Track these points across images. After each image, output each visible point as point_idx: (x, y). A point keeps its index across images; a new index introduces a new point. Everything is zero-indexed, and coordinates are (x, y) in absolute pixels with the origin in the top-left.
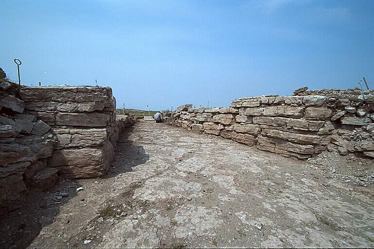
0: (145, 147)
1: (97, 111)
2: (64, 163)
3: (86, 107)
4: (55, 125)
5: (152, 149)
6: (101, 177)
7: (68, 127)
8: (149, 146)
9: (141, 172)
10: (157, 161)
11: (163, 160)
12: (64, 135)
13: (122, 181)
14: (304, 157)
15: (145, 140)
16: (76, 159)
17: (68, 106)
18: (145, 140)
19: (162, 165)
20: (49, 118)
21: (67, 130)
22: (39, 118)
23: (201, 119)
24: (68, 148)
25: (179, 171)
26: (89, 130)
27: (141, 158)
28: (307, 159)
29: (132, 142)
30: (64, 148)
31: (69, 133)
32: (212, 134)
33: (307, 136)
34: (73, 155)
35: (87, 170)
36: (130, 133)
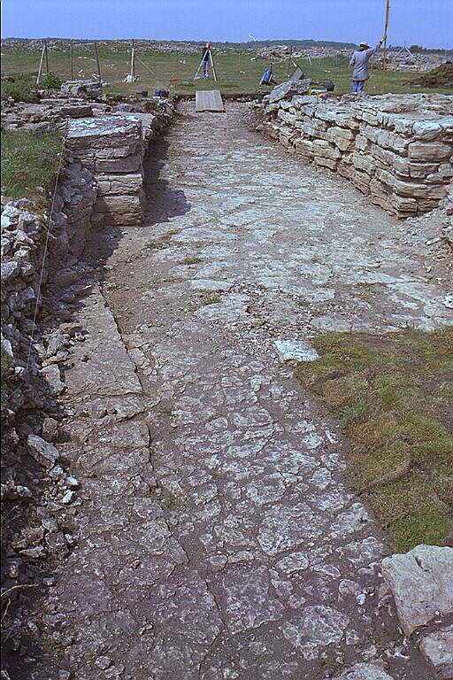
0: (187, 192)
1: (130, 155)
2: (106, 209)
3: (120, 152)
4: (95, 172)
5: (197, 196)
6: (139, 225)
7: (106, 173)
8: (193, 191)
9: (177, 222)
10: (200, 211)
11: (208, 212)
12: (104, 182)
13: (159, 230)
14: (406, 213)
15: (190, 178)
16: (116, 206)
17: (106, 152)
18: (190, 178)
19: (204, 216)
20: (90, 165)
21: (106, 177)
22: (83, 166)
23: (311, 132)
24: (108, 195)
25: (222, 224)
26: (126, 177)
27: (178, 206)
28: (406, 218)
29: (167, 182)
30: (106, 195)
31: (108, 180)
32: (325, 167)
33: (408, 185)
34: (115, 202)
35: (127, 216)
36: (161, 161)
